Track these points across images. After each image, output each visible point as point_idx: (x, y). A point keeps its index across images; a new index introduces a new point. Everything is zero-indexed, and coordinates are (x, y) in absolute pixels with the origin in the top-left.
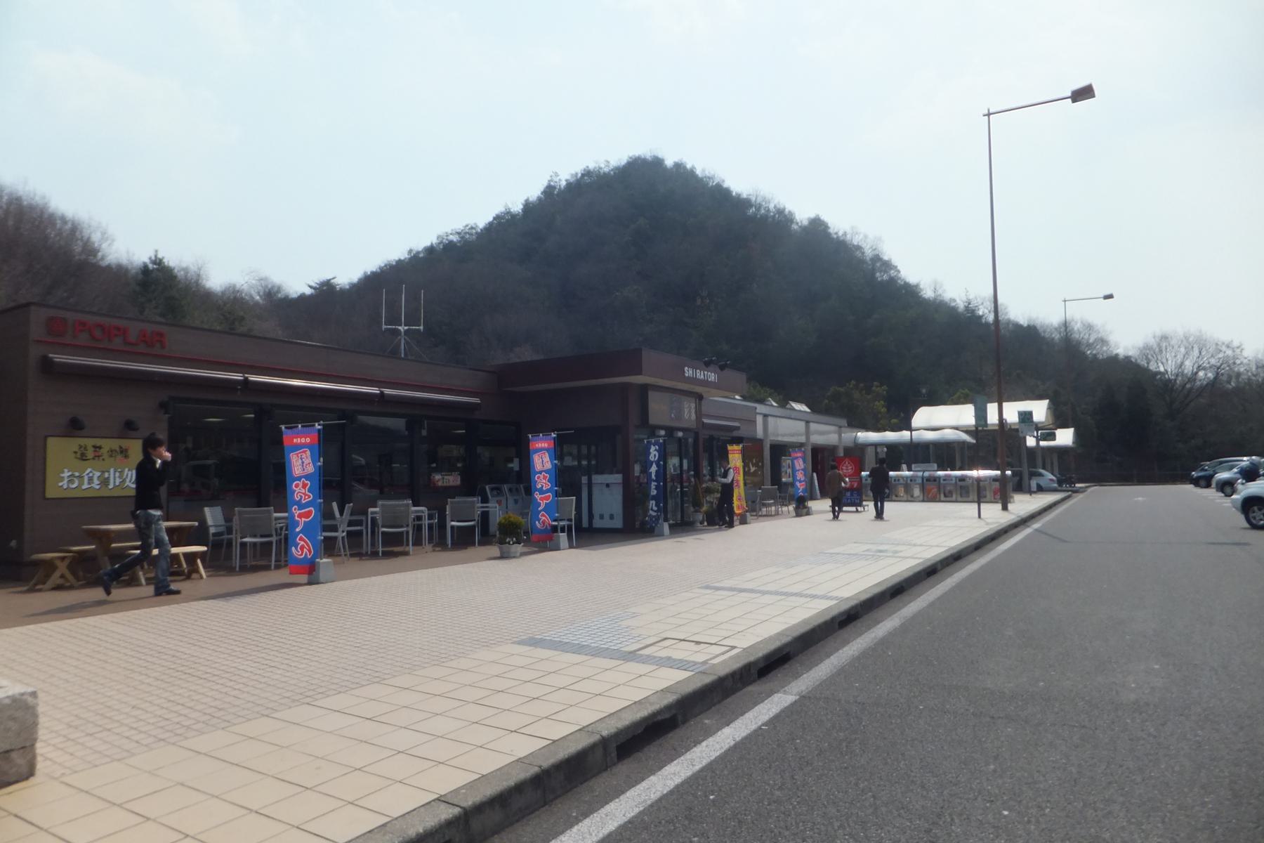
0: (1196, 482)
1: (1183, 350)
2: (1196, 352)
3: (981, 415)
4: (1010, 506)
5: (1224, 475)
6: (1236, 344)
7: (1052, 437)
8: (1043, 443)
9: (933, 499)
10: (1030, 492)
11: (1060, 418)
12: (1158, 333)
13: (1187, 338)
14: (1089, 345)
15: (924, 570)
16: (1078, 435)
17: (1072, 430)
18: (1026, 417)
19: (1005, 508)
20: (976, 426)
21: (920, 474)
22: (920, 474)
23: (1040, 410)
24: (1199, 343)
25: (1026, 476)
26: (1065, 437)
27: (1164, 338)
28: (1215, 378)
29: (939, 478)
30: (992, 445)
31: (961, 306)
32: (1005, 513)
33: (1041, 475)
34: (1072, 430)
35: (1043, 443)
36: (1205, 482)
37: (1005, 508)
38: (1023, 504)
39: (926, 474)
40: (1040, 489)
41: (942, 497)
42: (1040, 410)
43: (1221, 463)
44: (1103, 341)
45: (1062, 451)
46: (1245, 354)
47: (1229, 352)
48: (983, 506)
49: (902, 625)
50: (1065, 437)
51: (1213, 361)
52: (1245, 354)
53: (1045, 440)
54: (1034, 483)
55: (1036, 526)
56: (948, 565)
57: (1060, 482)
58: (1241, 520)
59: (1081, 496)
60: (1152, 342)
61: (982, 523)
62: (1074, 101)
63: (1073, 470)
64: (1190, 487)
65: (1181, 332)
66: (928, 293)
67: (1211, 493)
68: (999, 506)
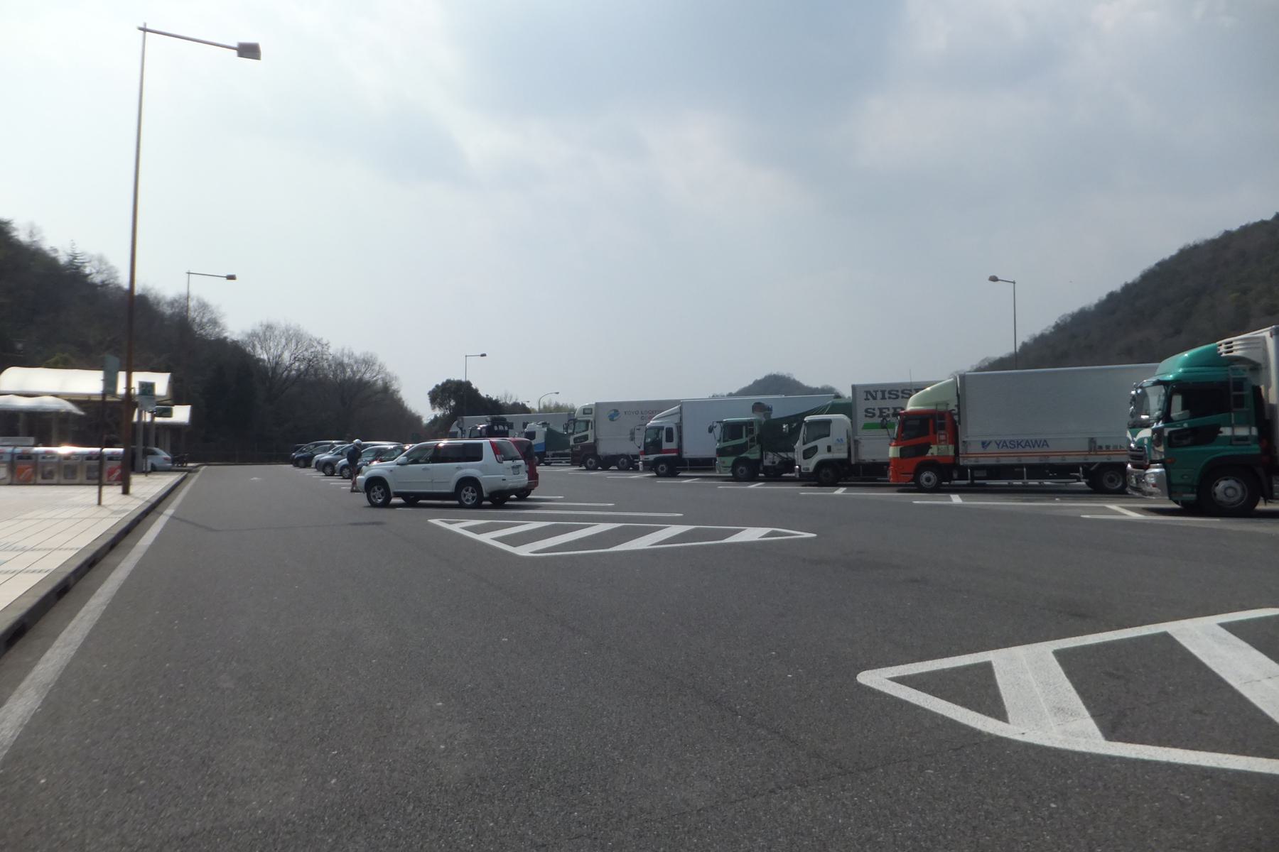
0: (296, 463)
1: (283, 341)
2: (293, 346)
3: (110, 383)
4: (132, 489)
5: (326, 457)
6: (324, 341)
7: (168, 413)
8: (158, 420)
9: (27, 482)
10: (146, 473)
11: (178, 396)
12: (265, 323)
13: (288, 330)
14: (202, 326)
15: (53, 591)
16: (194, 414)
17: (188, 407)
18: (147, 388)
19: (126, 491)
20: (104, 394)
21: (9, 449)
22: (9, 449)
23: (162, 383)
24: (294, 337)
25: (140, 454)
26: (181, 414)
27: (269, 327)
28: (307, 370)
29: (37, 454)
30: (98, 419)
31: (63, 259)
32: (127, 499)
33: (154, 453)
34: (188, 407)
35: (158, 420)
36: (306, 462)
37: (126, 491)
38: (147, 487)
39: (19, 450)
40: (154, 470)
41: (39, 479)
42: (162, 383)
43: (317, 445)
44: (214, 323)
45: (176, 429)
46: (331, 351)
47: (319, 348)
48: (106, 490)
49: (46, 703)
50: (181, 414)
51: (307, 354)
52: (331, 351)
53: (160, 416)
54: (150, 460)
55: (169, 512)
56: (82, 575)
57: (173, 461)
58: (362, 498)
59: (197, 476)
60: (259, 330)
61: (104, 513)
62: (241, 55)
63: (188, 448)
64: (289, 467)
65: (283, 324)
66: (22, 236)
67: (311, 473)
68: (119, 489)
